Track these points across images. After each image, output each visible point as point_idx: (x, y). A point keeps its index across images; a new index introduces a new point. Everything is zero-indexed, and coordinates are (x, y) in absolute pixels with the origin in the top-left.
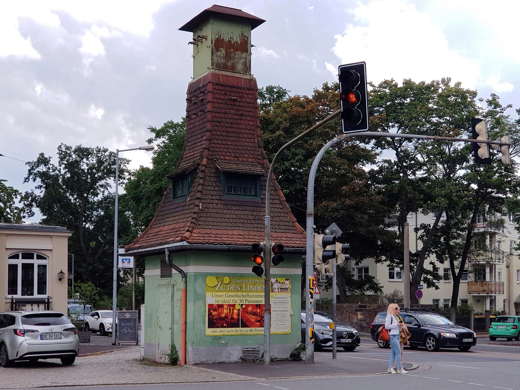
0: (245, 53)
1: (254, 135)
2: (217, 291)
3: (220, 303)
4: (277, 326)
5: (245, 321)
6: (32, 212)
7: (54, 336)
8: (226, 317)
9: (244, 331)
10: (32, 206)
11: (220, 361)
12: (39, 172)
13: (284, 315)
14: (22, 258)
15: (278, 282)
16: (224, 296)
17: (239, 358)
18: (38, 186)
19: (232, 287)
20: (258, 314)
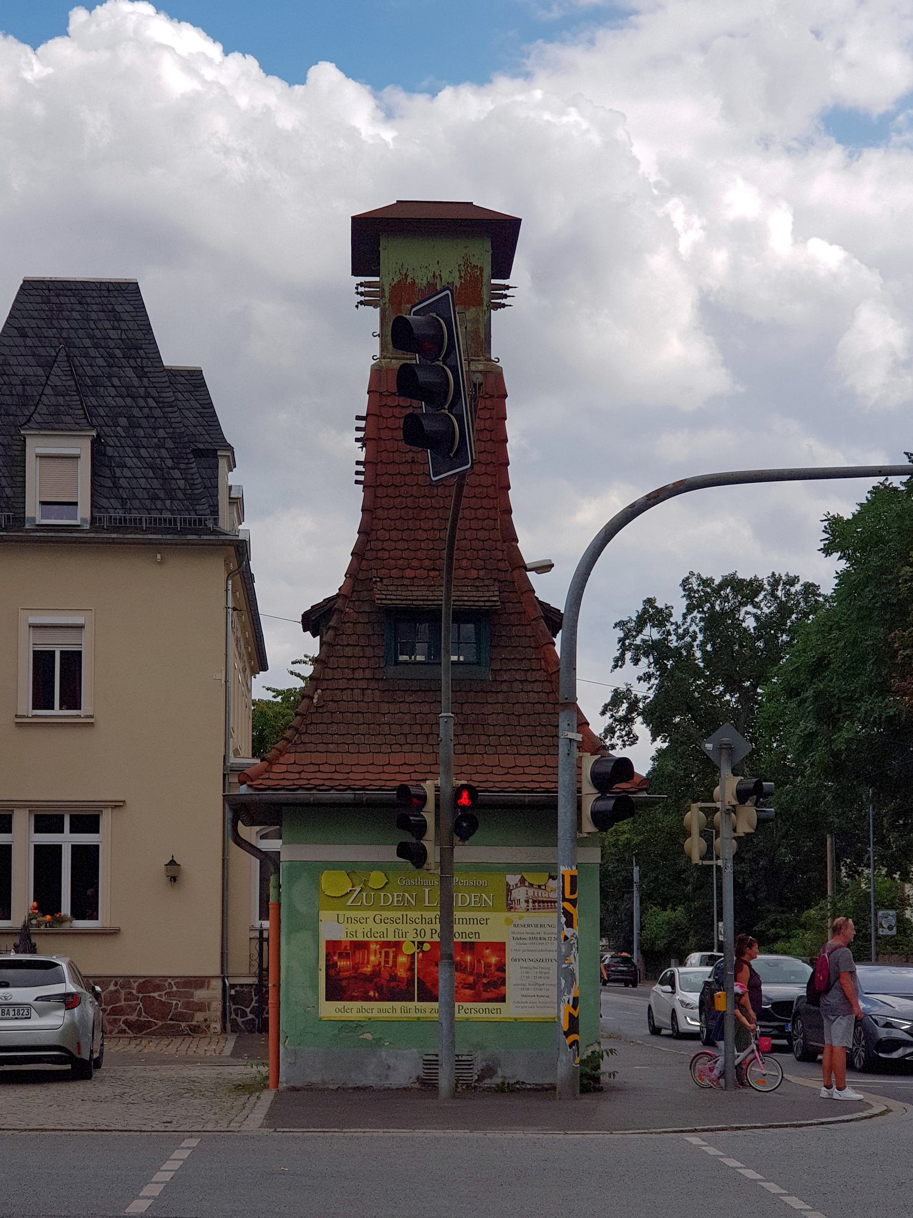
0: (473, 309)
1: (493, 511)
2: (350, 908)
3: (360, 938)
4: (525, 999)
5: (428, 985)
6: (631, 736)
7: (12, 1013)
8: (376, 973)
9: (428, 1011)
10: (632, 720)
11: (360, 1085)
12: (644, 641)
13: (547, 971)
14: (71, 832)
15: (527, 884)
16: (370, 921)
17: (414, 1079)
18: (644, 674)
19: (393, 897)
20: (466, 968)
